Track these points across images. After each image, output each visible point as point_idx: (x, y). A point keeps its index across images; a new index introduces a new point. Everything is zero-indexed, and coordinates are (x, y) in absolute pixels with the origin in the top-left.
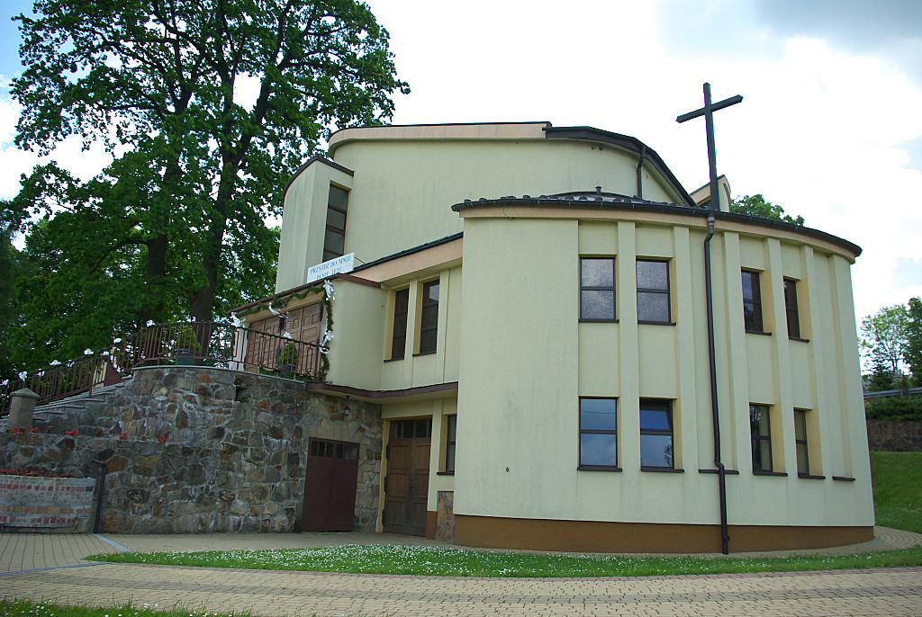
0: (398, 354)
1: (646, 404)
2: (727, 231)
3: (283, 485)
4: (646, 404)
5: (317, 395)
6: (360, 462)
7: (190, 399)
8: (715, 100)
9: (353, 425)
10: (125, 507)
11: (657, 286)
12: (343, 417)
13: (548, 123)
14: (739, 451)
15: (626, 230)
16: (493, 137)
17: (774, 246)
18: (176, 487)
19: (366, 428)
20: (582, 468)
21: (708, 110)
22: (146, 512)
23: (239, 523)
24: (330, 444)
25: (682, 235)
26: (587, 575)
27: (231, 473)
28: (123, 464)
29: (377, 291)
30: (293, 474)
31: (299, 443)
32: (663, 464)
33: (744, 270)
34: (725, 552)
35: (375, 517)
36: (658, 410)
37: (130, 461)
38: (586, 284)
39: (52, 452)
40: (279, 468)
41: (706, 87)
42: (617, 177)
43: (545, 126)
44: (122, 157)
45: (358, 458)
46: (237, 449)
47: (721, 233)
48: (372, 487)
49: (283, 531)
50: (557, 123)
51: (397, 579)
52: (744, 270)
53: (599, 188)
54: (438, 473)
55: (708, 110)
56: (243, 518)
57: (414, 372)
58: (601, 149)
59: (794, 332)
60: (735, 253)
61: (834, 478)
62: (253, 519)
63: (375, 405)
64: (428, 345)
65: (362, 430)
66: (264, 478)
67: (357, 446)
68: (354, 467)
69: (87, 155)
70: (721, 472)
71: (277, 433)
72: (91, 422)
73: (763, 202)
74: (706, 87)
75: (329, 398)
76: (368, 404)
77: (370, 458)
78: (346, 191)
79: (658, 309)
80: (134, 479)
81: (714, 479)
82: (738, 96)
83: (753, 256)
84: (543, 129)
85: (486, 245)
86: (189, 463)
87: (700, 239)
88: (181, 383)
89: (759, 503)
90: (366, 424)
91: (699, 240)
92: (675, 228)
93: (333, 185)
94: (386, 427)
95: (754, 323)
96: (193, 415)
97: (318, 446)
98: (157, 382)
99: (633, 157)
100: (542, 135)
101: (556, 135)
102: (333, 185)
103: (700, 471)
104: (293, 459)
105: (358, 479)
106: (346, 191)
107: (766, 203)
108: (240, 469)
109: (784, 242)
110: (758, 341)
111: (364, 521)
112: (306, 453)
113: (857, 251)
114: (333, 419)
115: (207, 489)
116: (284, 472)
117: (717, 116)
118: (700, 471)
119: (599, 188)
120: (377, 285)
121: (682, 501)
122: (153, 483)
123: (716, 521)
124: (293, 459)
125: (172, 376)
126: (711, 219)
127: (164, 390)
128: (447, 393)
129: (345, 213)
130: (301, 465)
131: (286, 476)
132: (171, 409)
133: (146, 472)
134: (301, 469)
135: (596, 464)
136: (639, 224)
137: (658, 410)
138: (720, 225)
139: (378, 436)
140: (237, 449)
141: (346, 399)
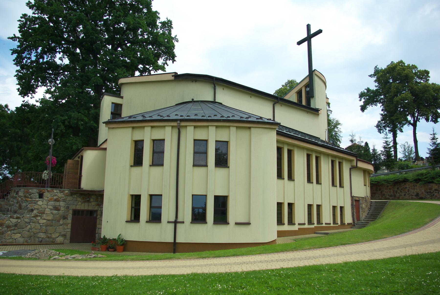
9: (93, 203)
13: (175, 73)
14: (186, 213)
15: (148, 130)
17: (233, 130)
25: (168, 130)
26: (111, 260)
41: (308, 26)
43: (174, 74)
45: (97, 215)
50: (179, 73)
51: (178, 273)
53: (193, 99)
54: (127, 222)
58: (196, 82)
61: (236, 224)
73: (404, 64)
74: (308, 26)
83: (201, 135)
84: (173, 76)
89: (191, 233)
91: (176, 131)
93: (122, 98)
99: (210, 83)
100: (173, 78)
107: (406, 65)
109: (237, 127)
110: (200, 171)
118: (168, 222)
121: (161, 233)
123: (173, 241)
126: (179, 122)
138: (183, 124)
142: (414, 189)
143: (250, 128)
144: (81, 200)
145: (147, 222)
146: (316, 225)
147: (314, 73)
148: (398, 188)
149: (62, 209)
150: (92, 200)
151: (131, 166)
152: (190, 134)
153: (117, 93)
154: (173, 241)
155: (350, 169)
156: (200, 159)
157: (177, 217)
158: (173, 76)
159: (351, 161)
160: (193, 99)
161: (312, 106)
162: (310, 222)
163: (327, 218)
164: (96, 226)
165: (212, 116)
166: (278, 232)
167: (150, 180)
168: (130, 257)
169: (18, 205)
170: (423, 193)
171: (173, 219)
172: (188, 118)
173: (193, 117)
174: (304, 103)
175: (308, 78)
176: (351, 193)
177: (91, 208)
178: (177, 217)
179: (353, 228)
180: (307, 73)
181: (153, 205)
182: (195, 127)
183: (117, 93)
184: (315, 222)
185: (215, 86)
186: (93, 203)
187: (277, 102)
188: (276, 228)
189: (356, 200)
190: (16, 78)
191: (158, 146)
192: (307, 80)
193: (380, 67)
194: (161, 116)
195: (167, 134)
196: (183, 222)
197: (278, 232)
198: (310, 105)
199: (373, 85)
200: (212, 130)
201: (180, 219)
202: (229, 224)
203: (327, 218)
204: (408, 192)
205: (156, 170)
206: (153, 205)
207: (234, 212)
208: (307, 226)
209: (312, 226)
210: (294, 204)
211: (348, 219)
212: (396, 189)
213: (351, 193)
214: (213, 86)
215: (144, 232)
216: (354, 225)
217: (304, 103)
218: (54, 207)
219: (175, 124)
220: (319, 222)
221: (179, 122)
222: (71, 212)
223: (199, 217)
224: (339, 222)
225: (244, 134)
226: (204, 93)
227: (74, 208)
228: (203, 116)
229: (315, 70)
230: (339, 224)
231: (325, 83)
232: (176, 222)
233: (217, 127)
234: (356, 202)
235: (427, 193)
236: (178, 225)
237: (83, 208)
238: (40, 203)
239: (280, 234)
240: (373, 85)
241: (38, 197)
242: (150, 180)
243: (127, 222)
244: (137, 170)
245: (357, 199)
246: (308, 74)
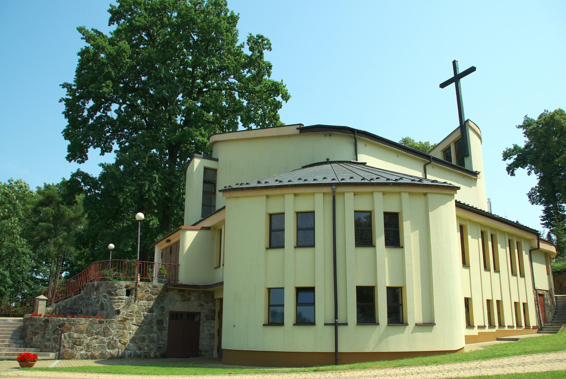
2: (347, 192)
3: (155, 335)
4: (299, 290)
5: (171, 290)
6: (201, 322)
7: (105, 297)
8: (460, 70)
10: (72, 348)
12: (189, 300)
17: (405, 197)
18: (96, 339)
19: (205, 304)
21: (456, 78)
22: (82, 350)
23: (131, 354)
24: (182, 314)
26: (148, 374)
27: (125, 331)
28: (70, 330)
29: (208, 231)
30: (161, 329)
31: (163, 314)
32: (304, 320)
35: (212, 350)
36: (306, 294)
37: (73, 327)
39: (40, 325)
40: (152, 327)
43: (298, 126)
45: (200, 320)
46: (128, 319)
47: (343, 193)
48: (210, 334)
49: (156, 357)
50: (307, 123)
53: (328, 159)
55: (456, 78)
56: (133, 352)
58: (330, 136)
62: (138, 352)
63: (210, 292)
65: (201, 305)
66: (144, 332)
67: (199, 313)
68: (198, 324)
69: (96, 162)
70: (336, 325)
72: (71, 309)
75: (180, 291)
76: (204, 292)
77: (207, 319)
78: (215, 170)
79: (306, 238)
80: (76, 335)
82: (473, 67)
83: (363, 205)
84: (297, 129)
86: (103, 327)
88: (101, 289)
90: (204, 302)
96: (106, 304)
98: (93, 289)
99: (351, 137)
100: (298, 132)
104: (160, 322)
105: (201, 330)
106: (215, 170)
108: (130, 328)
110: (365, 251)
111: (206, 352)
112: (168, 319)
115: (113, 338)
116: (155, 328)
117: (462, 81)
118: (326, 324)
120: (208, 228)
121: (315, 339)
122: (85, 337)
123: (333, 350)
125: (98, 286)
127: (95, 293)
130: (165, 325)
131: (156, 331)
132: (98, 301)
133: (81, 332)
134: (165, 327)
137: (306, 294)
138: (339, 190)
139: (213, 308)
140: (128, 319)
143: (425, 194)
145: (294, 325)
146: (497, 328)
150: (193, 298)
151: (267, 248)
152: (350, 204)
153: (207, 152)
154: (333, 350)
155: (530, 251)
156: (364, 238)
157: (336, 317)
158: (297, 129)
159: (530, 241)
160: (328, 159)
161: (467, 167)
162: (491, 325)
163: (509, 319)
164: (199, 335)
165: (263, 182)
166: (466, 337)
167: (297, 267)
168: (312, 368)
171: (331, 320)
172: (290, 183)
173: (296, 182)
174: (454, 162)
175: (459, 130)
176: (534, 284)
177: (192, 310)
178: (336, 317)
179: (541, 333)
181: (299, 302)
182: (384, 193)
183: (207, 152)
184: (497, 324)
185: (356, 142)
187: (429, 163)
188: (465, 332)
189: (540, 295)
190: (522, 131)
191: (306, 222)
192: (458, 134)
193: (530, 116)
194: (280, 182)
195: (318, 204)
196: (346, 324)
197: (466, 337)
198: (464, 165)
199: (522, 141)
200: (378, 197)
201: (340, 320)
202: (407, 324)
203: (509, 319)
205: (305, 252)
206: (299, 302)
207: (414, 310)
208: (487, 330)
209: (494, 330)
210: (471, 298)
211: (533, 322)
213: (534, 284)
214: (354, 141)
215: (291, 338)
216: (541, 330)
217: (454, 162)
220: (501, 325)
224: (523, 325)
225: (419, 202)
226: (341, 149)
227: (172, 310)
228: (333, 179)
229: (468, 120)
230: (524, 327)
231: (480, 138)
232: (336, 325)
233: (410, 194)
234: (539, 296)
236: (340, 329)
237: (182, 310)
239: (469, 339)
240: (522, 141)
241: (125, 294)
242: (297, 267)
244: (275, 253)
245: (541, 292)
246: (459, 125)
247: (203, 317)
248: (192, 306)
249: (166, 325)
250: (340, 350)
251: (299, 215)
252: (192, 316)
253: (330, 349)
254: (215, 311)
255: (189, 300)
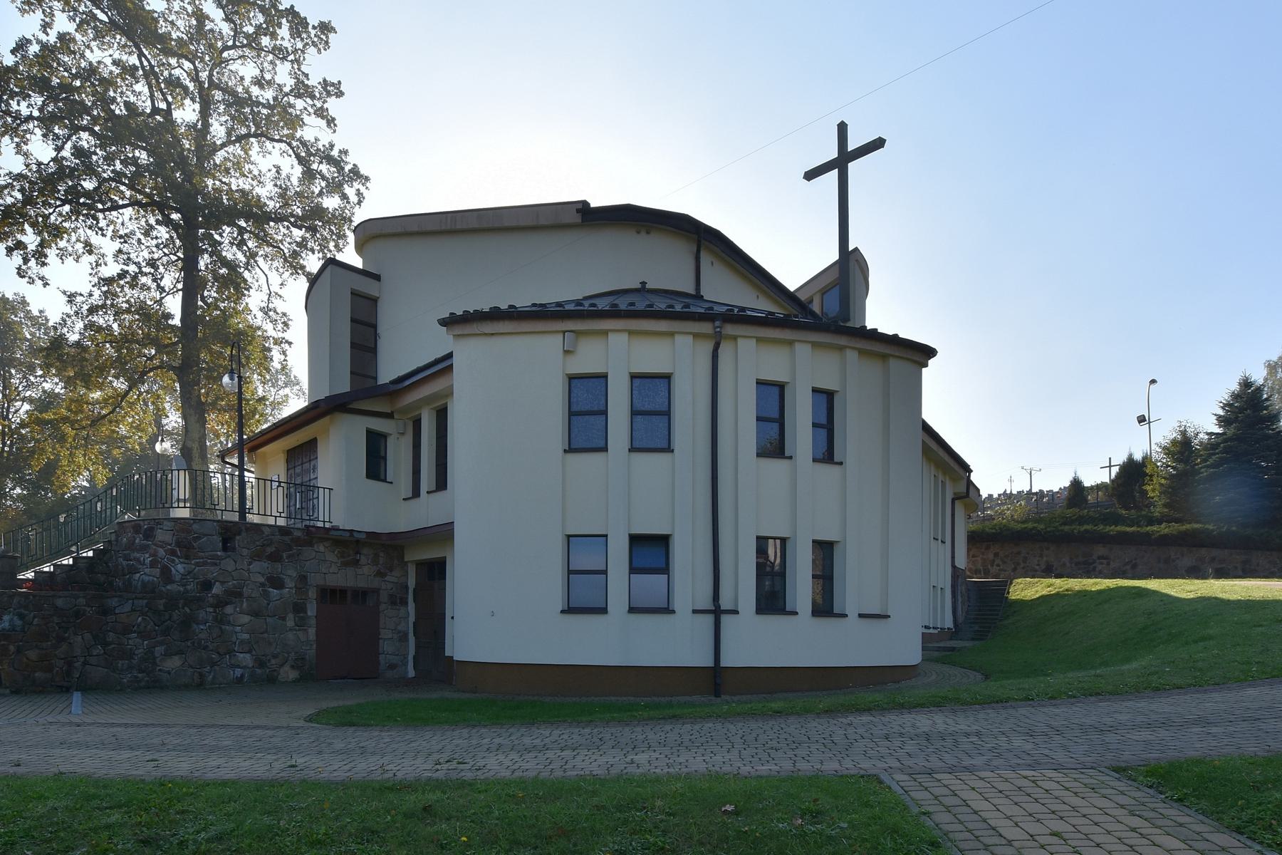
0: (416, 493)
1: (635, 540)
4: (635, 540)
11: (658, 408)
12: (356, 563)
16: (514, 224)
17: (852, 356)
20: (569, 610)
21: (842, 162)
30: (301, 624)
32: (824, 608)
33: (815, 390)
34: (717, 695)
35: (406, 664)
36: (651, 550)
38: (574, 408)
41: (842, 128)
42: (667, 269)
43: (580, 206)
44: (1264, 373)
47: (735, 338)
52: (815, 390)
53: (643, 283)
55: (842, 162)
57: (427, 512)
58: (648, 233)
59: (827, 455)
60: (752, 360)
61: (861, 616)
64: (441, 483)
67: (376, 591)
70: (717, 612)
71: (277, 583)
74: (842, 128)
78: (374, 301)
81: (709, 619)
85: (475, 360)
87: (708, 346)
89: (757, 643)
91: (706, 347)
92: (740, 341)
93: (355, 294)
94: (412, 571)
95: (774, 448)
97: (330, 595)
100: (577, 219)
101: (587, 217)
102: (355, 294)
103: (695, 612)
109: (862, 352)
113: (924, 353)
114: (346, 564)
118: (695, 612)
119: (643, 283)
121: (676, 643)
123: (710, 663)
124: (299, 609)
128: (444, 533)
129: (375, 327)
135: (582, 605)
136: (759, 340)
138: (730, 329)
141: (349, 544)
142: (1041, 556)
144: (335, 559)
147: (851, 257)
148: (996, 555)
149: (290, 583)
150: (363, 560)
169: (157, 571)
170: (1064, 564)
176: (953, 557)
177: (362, 584)
180: (835, 256)
185: (698, 251)
186: (366, 570)
192: (835, 274)
196: (736, 612)
201: (725, 603)
204: (1024, 562)
212: (991, 556)
213: (953, 557)
218: (268, 579)
219: (706, 328)
221: (717, 323)
222: (312, 594)
223: (772, 599)
232: (717, 612)
235: (1077, 564)
236: (725, 619)
238: (229, 565)
243: (563, 612)
247: (384, 597)
248: (361, 576)
249: (312, 610)
250: (725, 663)
251: (637, 382)
252: (362, 595)
253: (703, 659)
254: (407, 587)
255: (356, 563)
